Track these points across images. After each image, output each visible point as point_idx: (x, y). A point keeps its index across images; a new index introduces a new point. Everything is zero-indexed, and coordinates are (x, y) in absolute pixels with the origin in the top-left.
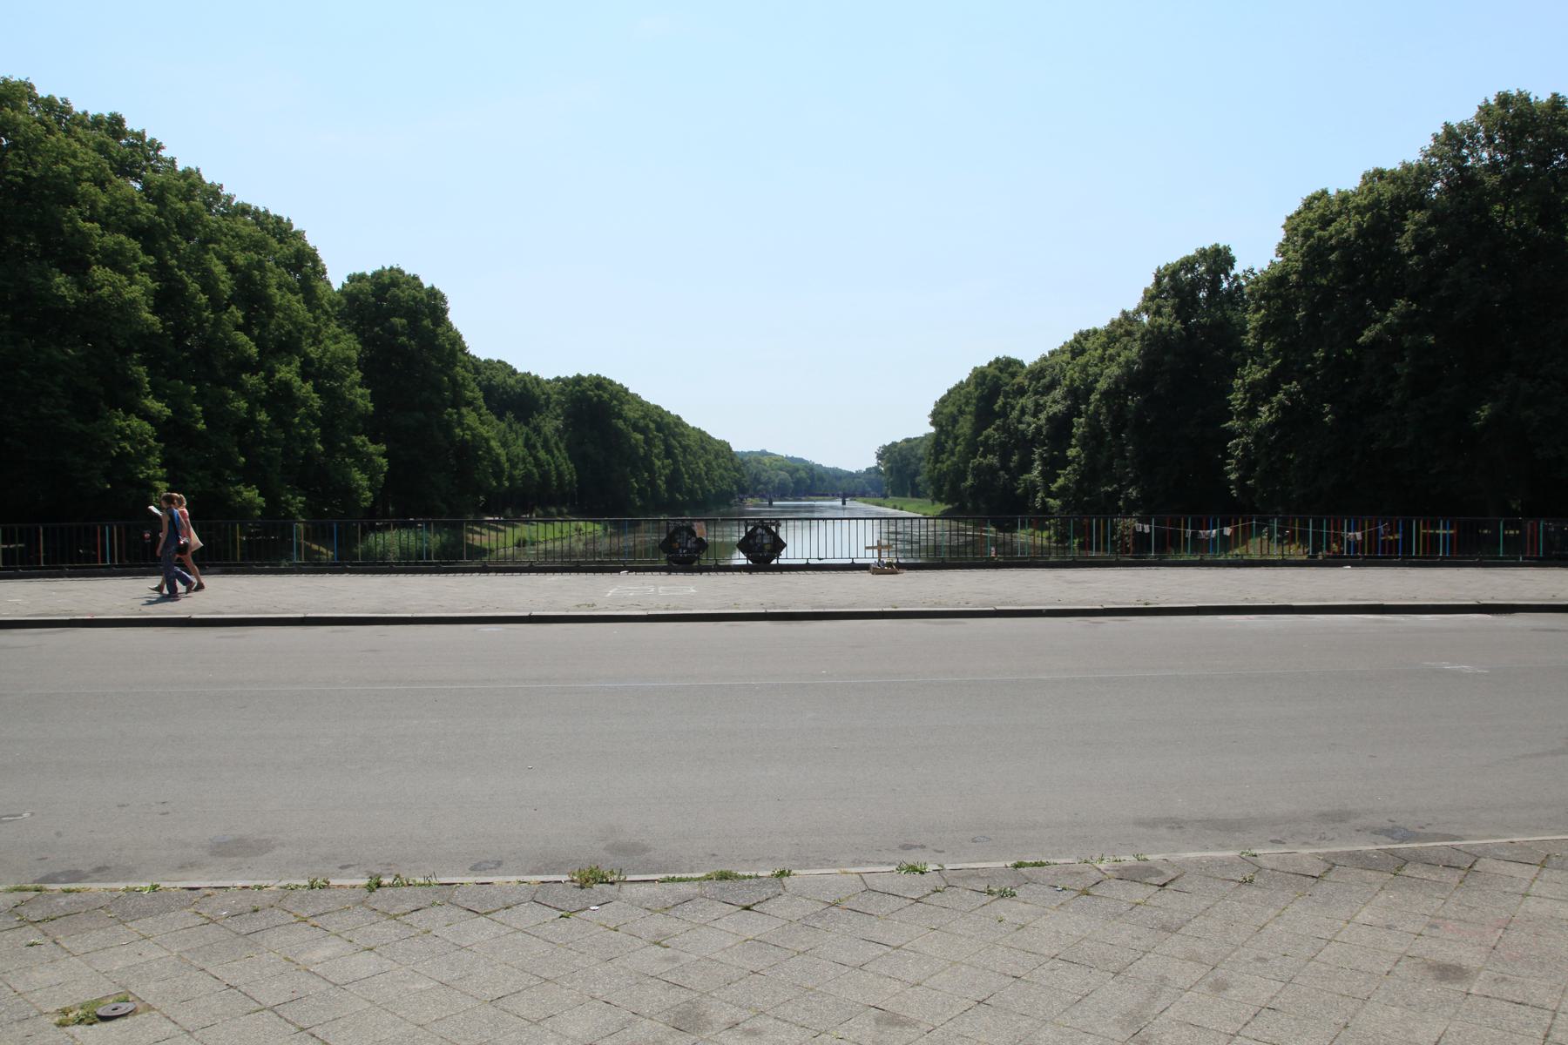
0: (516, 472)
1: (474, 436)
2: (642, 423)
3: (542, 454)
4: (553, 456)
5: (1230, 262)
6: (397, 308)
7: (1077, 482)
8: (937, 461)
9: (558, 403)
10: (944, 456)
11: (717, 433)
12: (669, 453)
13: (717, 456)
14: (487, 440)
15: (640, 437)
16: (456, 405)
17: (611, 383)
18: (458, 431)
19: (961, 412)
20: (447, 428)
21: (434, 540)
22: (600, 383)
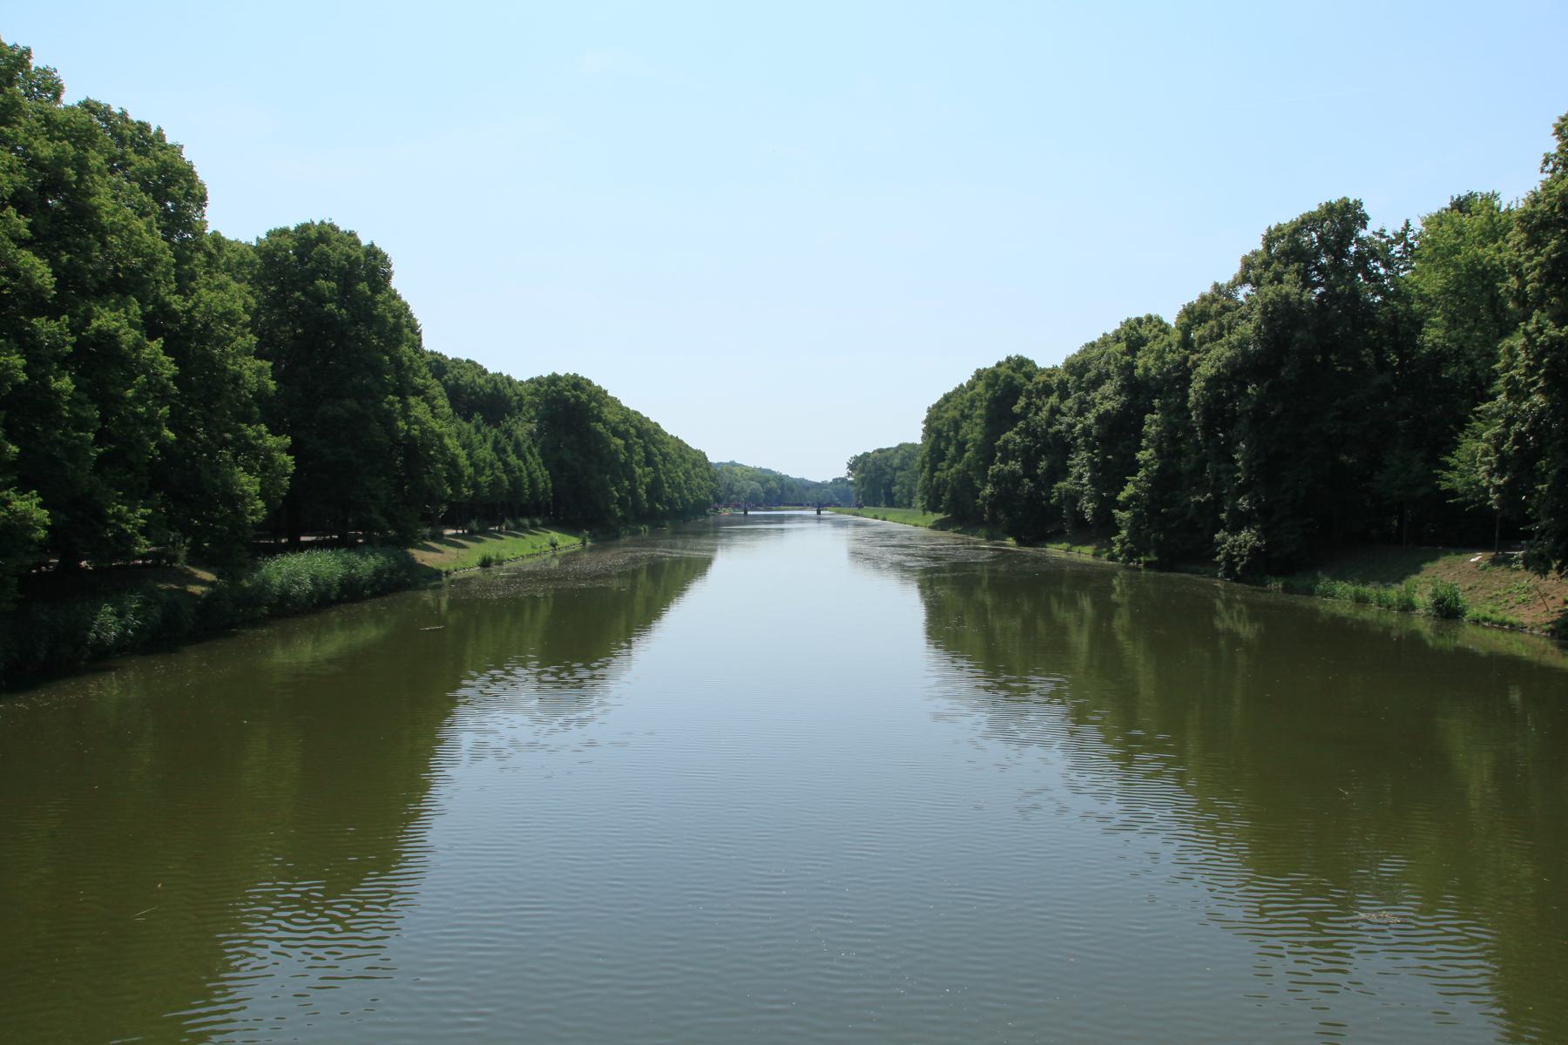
0: (482, 479)
1: (423, 432)
2: (622, 427)
3: (513, 459)
4: (525, 461)
5: (1363, 220)
6: (323, 267)
7: (1149, 490)
8: (934, 469)
9: (532, 404)
10: (944, 465)
11: (694, 444)
12: (649, 461)
13: (694, 465)
14: (440, 437)
15: (620, 442)
16: (401, 393)
17: (589, 383)
18: (401, 424)
19: (964, 417)
20: (387, 419)
21: (367, 564)
22: (577, 383)
